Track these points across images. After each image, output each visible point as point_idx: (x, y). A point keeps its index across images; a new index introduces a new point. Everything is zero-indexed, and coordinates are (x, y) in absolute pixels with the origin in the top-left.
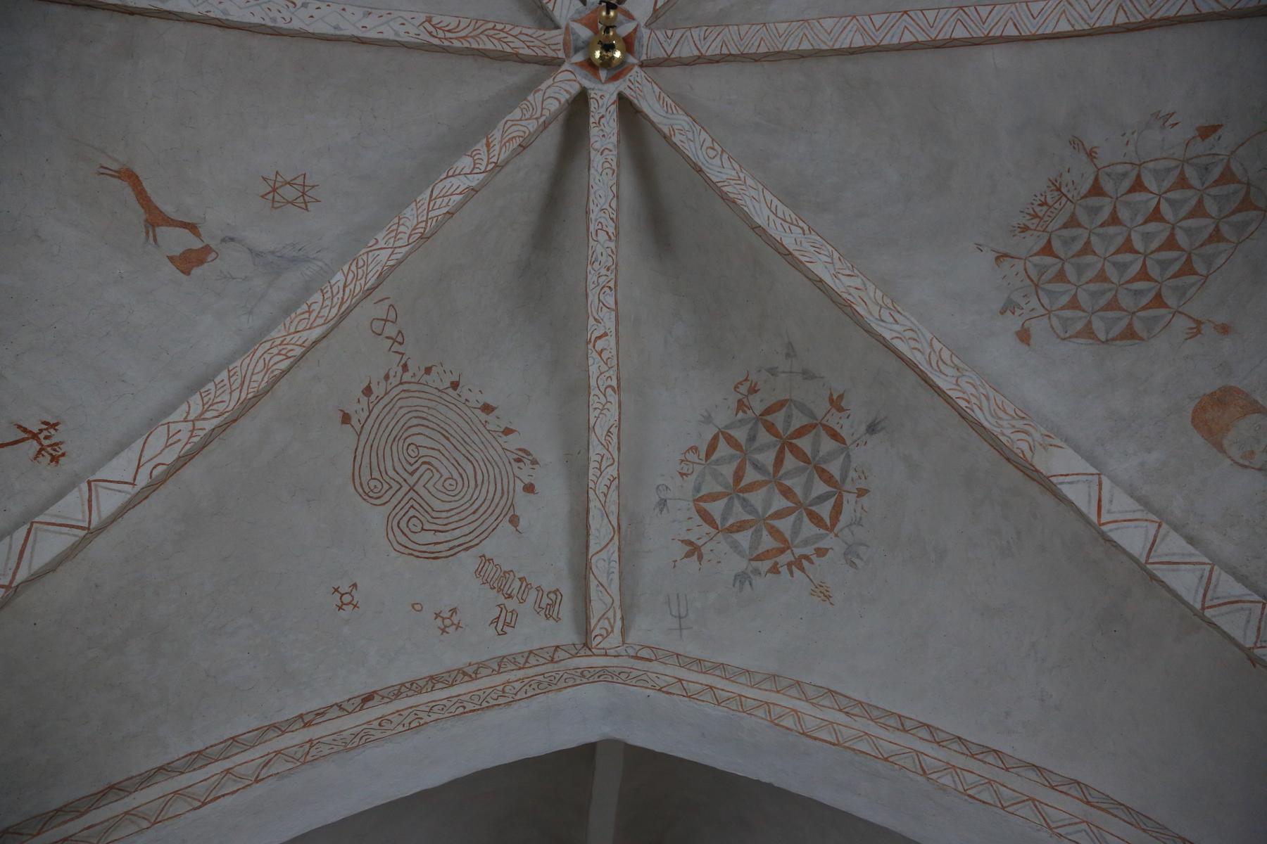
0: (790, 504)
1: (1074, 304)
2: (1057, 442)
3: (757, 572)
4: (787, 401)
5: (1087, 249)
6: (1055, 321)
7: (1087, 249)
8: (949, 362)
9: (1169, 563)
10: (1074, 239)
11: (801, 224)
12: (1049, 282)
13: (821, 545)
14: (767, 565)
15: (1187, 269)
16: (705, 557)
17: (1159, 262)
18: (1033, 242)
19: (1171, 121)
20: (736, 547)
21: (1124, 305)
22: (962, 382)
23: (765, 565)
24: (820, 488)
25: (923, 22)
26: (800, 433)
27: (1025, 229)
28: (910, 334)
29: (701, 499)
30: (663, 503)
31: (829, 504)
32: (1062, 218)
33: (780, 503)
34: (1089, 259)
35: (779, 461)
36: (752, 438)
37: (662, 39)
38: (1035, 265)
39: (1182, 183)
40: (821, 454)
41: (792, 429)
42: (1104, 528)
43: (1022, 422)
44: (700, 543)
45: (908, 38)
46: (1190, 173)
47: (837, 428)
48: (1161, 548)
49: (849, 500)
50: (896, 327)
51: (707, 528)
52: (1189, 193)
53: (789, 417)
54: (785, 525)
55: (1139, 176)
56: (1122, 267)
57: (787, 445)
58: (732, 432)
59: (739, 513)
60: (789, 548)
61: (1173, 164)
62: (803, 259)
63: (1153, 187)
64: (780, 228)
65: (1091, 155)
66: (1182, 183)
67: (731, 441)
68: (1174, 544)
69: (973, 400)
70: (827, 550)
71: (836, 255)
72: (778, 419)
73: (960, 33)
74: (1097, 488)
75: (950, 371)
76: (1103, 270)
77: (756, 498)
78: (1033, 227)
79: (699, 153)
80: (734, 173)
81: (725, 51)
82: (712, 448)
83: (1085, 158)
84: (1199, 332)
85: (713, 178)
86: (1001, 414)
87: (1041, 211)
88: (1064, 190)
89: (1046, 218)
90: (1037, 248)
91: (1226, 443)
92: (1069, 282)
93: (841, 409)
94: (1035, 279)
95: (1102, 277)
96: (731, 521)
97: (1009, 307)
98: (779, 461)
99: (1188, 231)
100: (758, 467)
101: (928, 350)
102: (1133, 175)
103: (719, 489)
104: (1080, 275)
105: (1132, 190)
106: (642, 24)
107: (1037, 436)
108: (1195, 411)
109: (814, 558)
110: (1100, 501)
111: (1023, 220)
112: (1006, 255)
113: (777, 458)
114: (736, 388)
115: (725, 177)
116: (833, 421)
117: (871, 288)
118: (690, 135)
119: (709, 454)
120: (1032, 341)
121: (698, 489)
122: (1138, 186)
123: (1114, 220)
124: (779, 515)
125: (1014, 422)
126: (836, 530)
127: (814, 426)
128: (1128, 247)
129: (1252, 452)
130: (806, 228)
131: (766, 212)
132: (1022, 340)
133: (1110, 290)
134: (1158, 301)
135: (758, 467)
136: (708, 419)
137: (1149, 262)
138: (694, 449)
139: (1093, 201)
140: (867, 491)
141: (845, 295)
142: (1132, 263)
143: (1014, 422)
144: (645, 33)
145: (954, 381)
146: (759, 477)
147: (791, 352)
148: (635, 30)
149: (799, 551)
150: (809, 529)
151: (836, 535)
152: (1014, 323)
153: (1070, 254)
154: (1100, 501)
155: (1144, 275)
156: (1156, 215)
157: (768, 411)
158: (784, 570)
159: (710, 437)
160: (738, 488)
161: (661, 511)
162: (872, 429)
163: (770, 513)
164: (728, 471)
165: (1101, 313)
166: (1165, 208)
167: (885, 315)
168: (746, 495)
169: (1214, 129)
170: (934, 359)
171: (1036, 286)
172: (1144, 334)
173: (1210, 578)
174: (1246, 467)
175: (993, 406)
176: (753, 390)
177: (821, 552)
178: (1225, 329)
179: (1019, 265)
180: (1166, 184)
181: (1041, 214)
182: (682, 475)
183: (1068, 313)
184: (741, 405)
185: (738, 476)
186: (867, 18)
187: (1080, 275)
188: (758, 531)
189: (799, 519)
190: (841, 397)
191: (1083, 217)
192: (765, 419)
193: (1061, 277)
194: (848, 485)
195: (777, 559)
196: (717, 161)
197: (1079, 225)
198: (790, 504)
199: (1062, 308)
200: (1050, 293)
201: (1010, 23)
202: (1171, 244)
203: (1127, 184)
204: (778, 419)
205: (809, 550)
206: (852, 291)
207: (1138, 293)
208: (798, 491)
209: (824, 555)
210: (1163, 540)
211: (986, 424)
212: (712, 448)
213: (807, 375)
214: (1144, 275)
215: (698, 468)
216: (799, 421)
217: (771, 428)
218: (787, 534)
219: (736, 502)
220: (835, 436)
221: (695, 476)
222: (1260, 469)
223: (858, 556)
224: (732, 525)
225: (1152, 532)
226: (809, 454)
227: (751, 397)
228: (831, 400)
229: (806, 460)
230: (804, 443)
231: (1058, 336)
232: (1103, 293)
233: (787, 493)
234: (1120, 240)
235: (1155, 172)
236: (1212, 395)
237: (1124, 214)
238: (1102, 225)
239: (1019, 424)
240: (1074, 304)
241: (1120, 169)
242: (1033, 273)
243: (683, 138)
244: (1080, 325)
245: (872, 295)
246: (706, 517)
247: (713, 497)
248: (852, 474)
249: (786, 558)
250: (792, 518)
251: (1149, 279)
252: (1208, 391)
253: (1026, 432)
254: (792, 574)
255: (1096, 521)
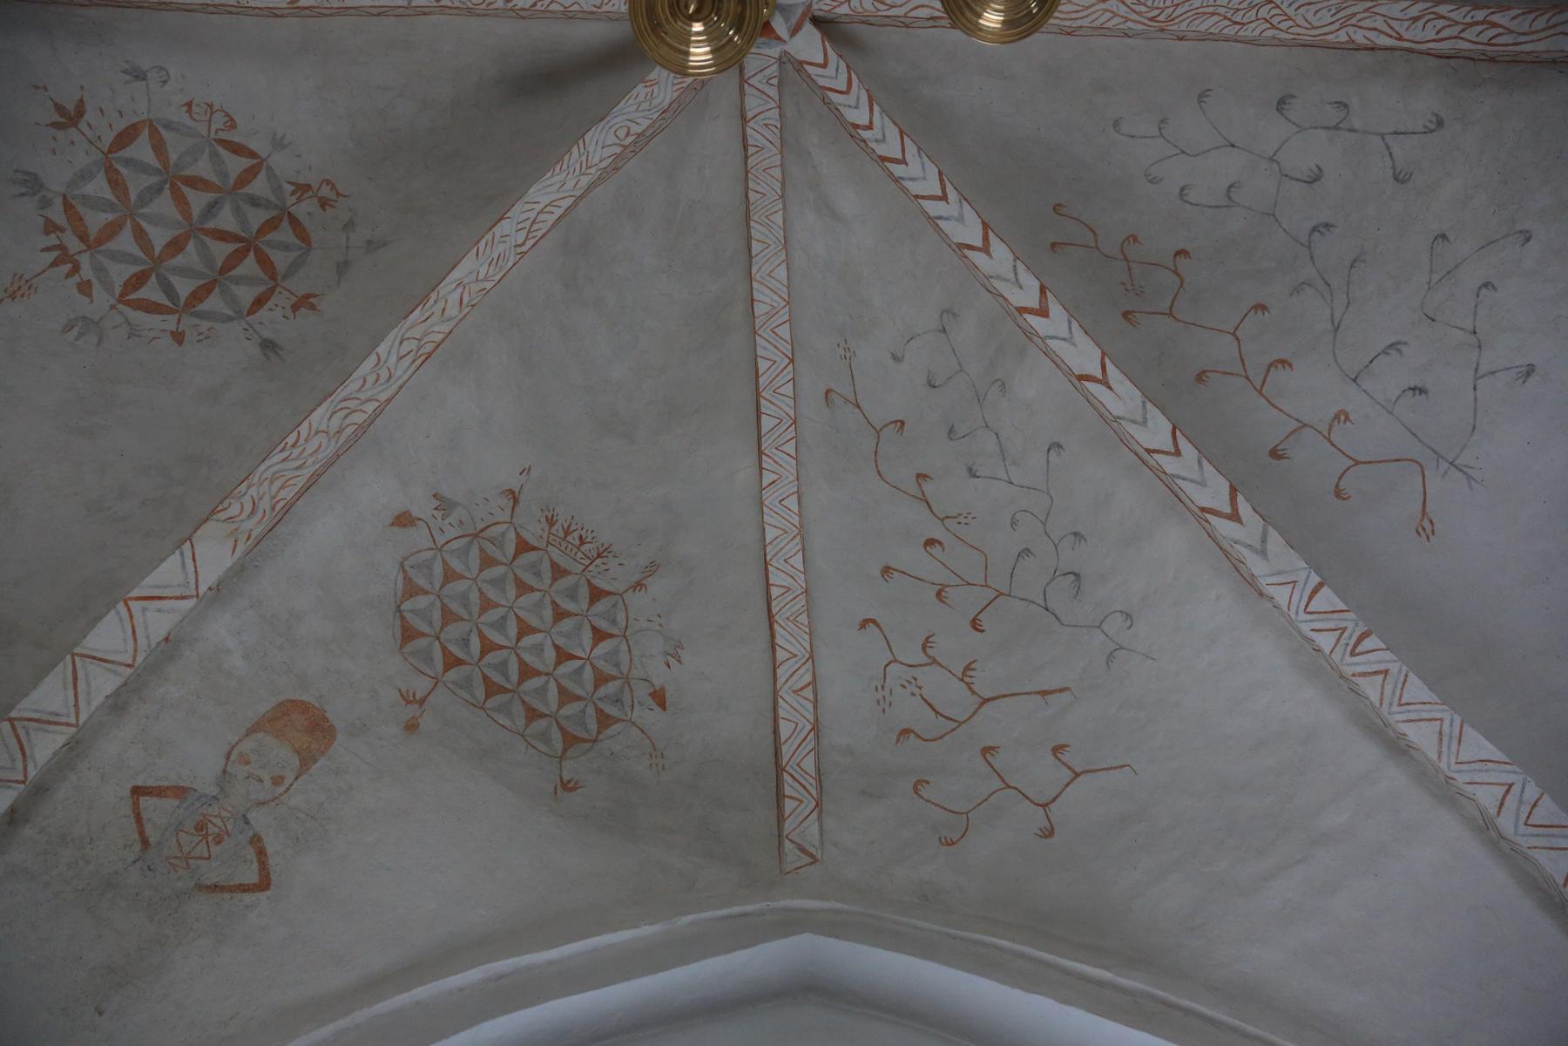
0: (158, 250)
1: (450, 576)
2: (241, 548)
3: (45, 204)
4: (309, 244)
5: (523, 588)
6: (429, 554)
7: (523, 588)
8: (347, 421)
9: (75, 679)
10: (538, 574)
11: (530, 243)
12: (482, 550)
13: (96, 285)
14: (58, 217)
15: (492, 689)
16: (60, 134)
17: (505, 663)
18: (534, 531)
19: (672, 661)
20: (85, 175)
21: (449, 628)
22: (322, 438)
23: (57, 214)
24: (184, 288)
25: (781, 380)
26: (264, 262)
27: (551, 522)
28: (384, 374)
29: (154, 132)
30: (139, 75)
31: (160, 297)
32: (563, 562)
33: (159, 238)
34: (512, 591)
35: (222, 236)
36: (255, 202)
37: (768, 72)
38: (503, 534)
39: (601, 679)
40: (233, 287)
41: (268, 251)
42: (121, 606)
43: (268, 508)
44: (83, 126)
45: (763, 365)
46: (611, 688)
47: (270, 304)
48: (94, 668)
49: (170, 322)
50: (393, 359)
51: (108, 138)
52: (590, 688)
53: (287, 247)
54: (125, 241)
55: (611, 636)
56: (500, 625)
57: (245, 246)
58: (262, 176)
59: (137, 184)
60: (89, 247)
61: (625, 669)
62: (482, 244)
63: (599, 650)
64: (524, 216)
65: (639, 585)
66: (601, 679)
67: (249, 175)
68: (103, 684)
69: (296, 452)
70: (89, 295)
71: (488, 285)
72: (285, 234)
73: (767, 423)
74: (178, 593)
75: (335, 422)
76: (497, 605)
77: (164, 205)
78: (554, 530)
79: (619, 119)
80: (596, 160)
81: (751, 150)
82: (237, 149)
83: (635, 579)
84: (408, 702)
85: (590, 134)
86: (278, 484)
87: (574, 538)
88: (598, 561)
89: (564, 544)
90: (524, 534)
91: (260, 735)
92: (481, 570)
93: (295, 308)
94: (486, 533)
95: (487, 605)
96: (124, 171)
97: (444, 505)
98: (222, 236)
99: (543, 689)
100: (211, 209)
101: (363, 396)
102: (614, 631)
103: (173, 157)
104: (492, 582)
105: (595, 629)
106: (786, 47)
107: (249, 524)
108: (303, 702)
109: (76, 279)
110: (160, 598)
111: (562, 521)
112: (516, 501)
113: (227, 232)
114: (328, 182)
115: (591, 149)
116: (280, 300)
117: (446, 328)
118: (645, 106)
119: (225, 143)
120: (396, 529)
121: (168, 126)
122: (599, 636)
123: (560, 615)
124: (140, 235)
125: (267, 498)
126: (120, 306)
127: (273, 277)
128: (525, 630)
129: (248, 763)
130: (524, 249)
131: (545, 200)
132: (398, 517)
133: (470, 614)
134: (452, 662)
135: (211, 209)
136: (278, 144)
137: (505, 653)
138: (232, 124)
139: (584, 592)
140: (180, 343)
141: (433, 296)
142: (506, 636)
143: (267, 498)
144: (775, 51)
145: (323, 427)
146: (196, 211)
147: (372, 245)
148: (779, 38)
149: (84, 260)
150: (120, 273)
151: (112, 307)
152: (422, 507)
153: (518, 572)
154: (160, 598)
155: (488, 647)
156: (563, 656)
157: (294, 222)
158: (53, 240)
159: (253, 146)
160: (178, 183)
161: (126, 72)
162: (268, 346)
163: (144, 224)
164: (202, 168)
165: (438, 604)
166: (573, 665)
167: (407, 347)
168: (167, 192)
169: (662, 704)
170: (352, 404)
171: (476, 535)
172: (408, 648)
173: (56, 723)
174: (228, 757)
175: (289, 475)
176: (324, 203)
177: (85, 288)
178: (411, 727)
179: (505, 517)
180: (601, 664)
181: (569, 538)
182: (189, 105)
183: (438, 569)
184: (302, 189)
185: (195, 182)
186: (786, 317)
187: (492, 582)
188: (112, 207)
189: (135, 261)
190: (313, 307)
191: (564, 583)
192: (283, 217)
193: (487, 562)
194: (188, 321)
195: (69, 232)
196: (611, 139)
197: (554, 579)
198: (158, 250)
199: (444, 562)
200: (465, 551)
201: (776, 477)
202: (527, 672)
203: (603, 625)
204: (285, 234)
205: (87, 272)
206: (441, 304)
207: (465, 643)
208: (179, 260)
209: (81, 292)
210: (110, 670)
211: (268, 463)
212: (237, 149)
213: (343, 267)
214: (488, 647)
215: (203, 130)
216: (280, 259)
217: (271, 225)
218: (112, 245)
219: (155, 179)
220: (259, 302)
221: (189, 122)
222: (224, 771)
223: (81, 334)
224: (117, 172)
225: (120, 658)
226: (232, 273)
227: (315, 201)
228: (308, 296)
229: (224, 270)
230: (249, 266)
231: (406, 559)
232: (466, 606)
233: (176, 246)
234: (534, 622)
235: (616, 651)
236: (327, 720)
237: (567, 625)
238: (554, 603)
239: (265, 504)
240: (450, 576)
241: (621, 617)
242: (495, 531)
243: (641, 98)
244: (421, 581)
245: (436, 328)
246: (126, 137)
247: (159, 147)
248: (205, 325)
249: (74, 244)
250: (137, 251)
251: (483, 654)
252: (328, 715)
253: (253, 512)
254: (48, 249)
255: (132, 595)
